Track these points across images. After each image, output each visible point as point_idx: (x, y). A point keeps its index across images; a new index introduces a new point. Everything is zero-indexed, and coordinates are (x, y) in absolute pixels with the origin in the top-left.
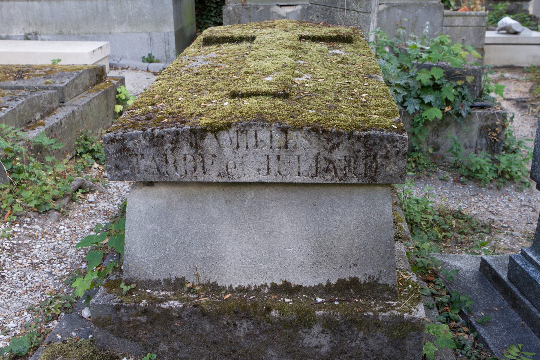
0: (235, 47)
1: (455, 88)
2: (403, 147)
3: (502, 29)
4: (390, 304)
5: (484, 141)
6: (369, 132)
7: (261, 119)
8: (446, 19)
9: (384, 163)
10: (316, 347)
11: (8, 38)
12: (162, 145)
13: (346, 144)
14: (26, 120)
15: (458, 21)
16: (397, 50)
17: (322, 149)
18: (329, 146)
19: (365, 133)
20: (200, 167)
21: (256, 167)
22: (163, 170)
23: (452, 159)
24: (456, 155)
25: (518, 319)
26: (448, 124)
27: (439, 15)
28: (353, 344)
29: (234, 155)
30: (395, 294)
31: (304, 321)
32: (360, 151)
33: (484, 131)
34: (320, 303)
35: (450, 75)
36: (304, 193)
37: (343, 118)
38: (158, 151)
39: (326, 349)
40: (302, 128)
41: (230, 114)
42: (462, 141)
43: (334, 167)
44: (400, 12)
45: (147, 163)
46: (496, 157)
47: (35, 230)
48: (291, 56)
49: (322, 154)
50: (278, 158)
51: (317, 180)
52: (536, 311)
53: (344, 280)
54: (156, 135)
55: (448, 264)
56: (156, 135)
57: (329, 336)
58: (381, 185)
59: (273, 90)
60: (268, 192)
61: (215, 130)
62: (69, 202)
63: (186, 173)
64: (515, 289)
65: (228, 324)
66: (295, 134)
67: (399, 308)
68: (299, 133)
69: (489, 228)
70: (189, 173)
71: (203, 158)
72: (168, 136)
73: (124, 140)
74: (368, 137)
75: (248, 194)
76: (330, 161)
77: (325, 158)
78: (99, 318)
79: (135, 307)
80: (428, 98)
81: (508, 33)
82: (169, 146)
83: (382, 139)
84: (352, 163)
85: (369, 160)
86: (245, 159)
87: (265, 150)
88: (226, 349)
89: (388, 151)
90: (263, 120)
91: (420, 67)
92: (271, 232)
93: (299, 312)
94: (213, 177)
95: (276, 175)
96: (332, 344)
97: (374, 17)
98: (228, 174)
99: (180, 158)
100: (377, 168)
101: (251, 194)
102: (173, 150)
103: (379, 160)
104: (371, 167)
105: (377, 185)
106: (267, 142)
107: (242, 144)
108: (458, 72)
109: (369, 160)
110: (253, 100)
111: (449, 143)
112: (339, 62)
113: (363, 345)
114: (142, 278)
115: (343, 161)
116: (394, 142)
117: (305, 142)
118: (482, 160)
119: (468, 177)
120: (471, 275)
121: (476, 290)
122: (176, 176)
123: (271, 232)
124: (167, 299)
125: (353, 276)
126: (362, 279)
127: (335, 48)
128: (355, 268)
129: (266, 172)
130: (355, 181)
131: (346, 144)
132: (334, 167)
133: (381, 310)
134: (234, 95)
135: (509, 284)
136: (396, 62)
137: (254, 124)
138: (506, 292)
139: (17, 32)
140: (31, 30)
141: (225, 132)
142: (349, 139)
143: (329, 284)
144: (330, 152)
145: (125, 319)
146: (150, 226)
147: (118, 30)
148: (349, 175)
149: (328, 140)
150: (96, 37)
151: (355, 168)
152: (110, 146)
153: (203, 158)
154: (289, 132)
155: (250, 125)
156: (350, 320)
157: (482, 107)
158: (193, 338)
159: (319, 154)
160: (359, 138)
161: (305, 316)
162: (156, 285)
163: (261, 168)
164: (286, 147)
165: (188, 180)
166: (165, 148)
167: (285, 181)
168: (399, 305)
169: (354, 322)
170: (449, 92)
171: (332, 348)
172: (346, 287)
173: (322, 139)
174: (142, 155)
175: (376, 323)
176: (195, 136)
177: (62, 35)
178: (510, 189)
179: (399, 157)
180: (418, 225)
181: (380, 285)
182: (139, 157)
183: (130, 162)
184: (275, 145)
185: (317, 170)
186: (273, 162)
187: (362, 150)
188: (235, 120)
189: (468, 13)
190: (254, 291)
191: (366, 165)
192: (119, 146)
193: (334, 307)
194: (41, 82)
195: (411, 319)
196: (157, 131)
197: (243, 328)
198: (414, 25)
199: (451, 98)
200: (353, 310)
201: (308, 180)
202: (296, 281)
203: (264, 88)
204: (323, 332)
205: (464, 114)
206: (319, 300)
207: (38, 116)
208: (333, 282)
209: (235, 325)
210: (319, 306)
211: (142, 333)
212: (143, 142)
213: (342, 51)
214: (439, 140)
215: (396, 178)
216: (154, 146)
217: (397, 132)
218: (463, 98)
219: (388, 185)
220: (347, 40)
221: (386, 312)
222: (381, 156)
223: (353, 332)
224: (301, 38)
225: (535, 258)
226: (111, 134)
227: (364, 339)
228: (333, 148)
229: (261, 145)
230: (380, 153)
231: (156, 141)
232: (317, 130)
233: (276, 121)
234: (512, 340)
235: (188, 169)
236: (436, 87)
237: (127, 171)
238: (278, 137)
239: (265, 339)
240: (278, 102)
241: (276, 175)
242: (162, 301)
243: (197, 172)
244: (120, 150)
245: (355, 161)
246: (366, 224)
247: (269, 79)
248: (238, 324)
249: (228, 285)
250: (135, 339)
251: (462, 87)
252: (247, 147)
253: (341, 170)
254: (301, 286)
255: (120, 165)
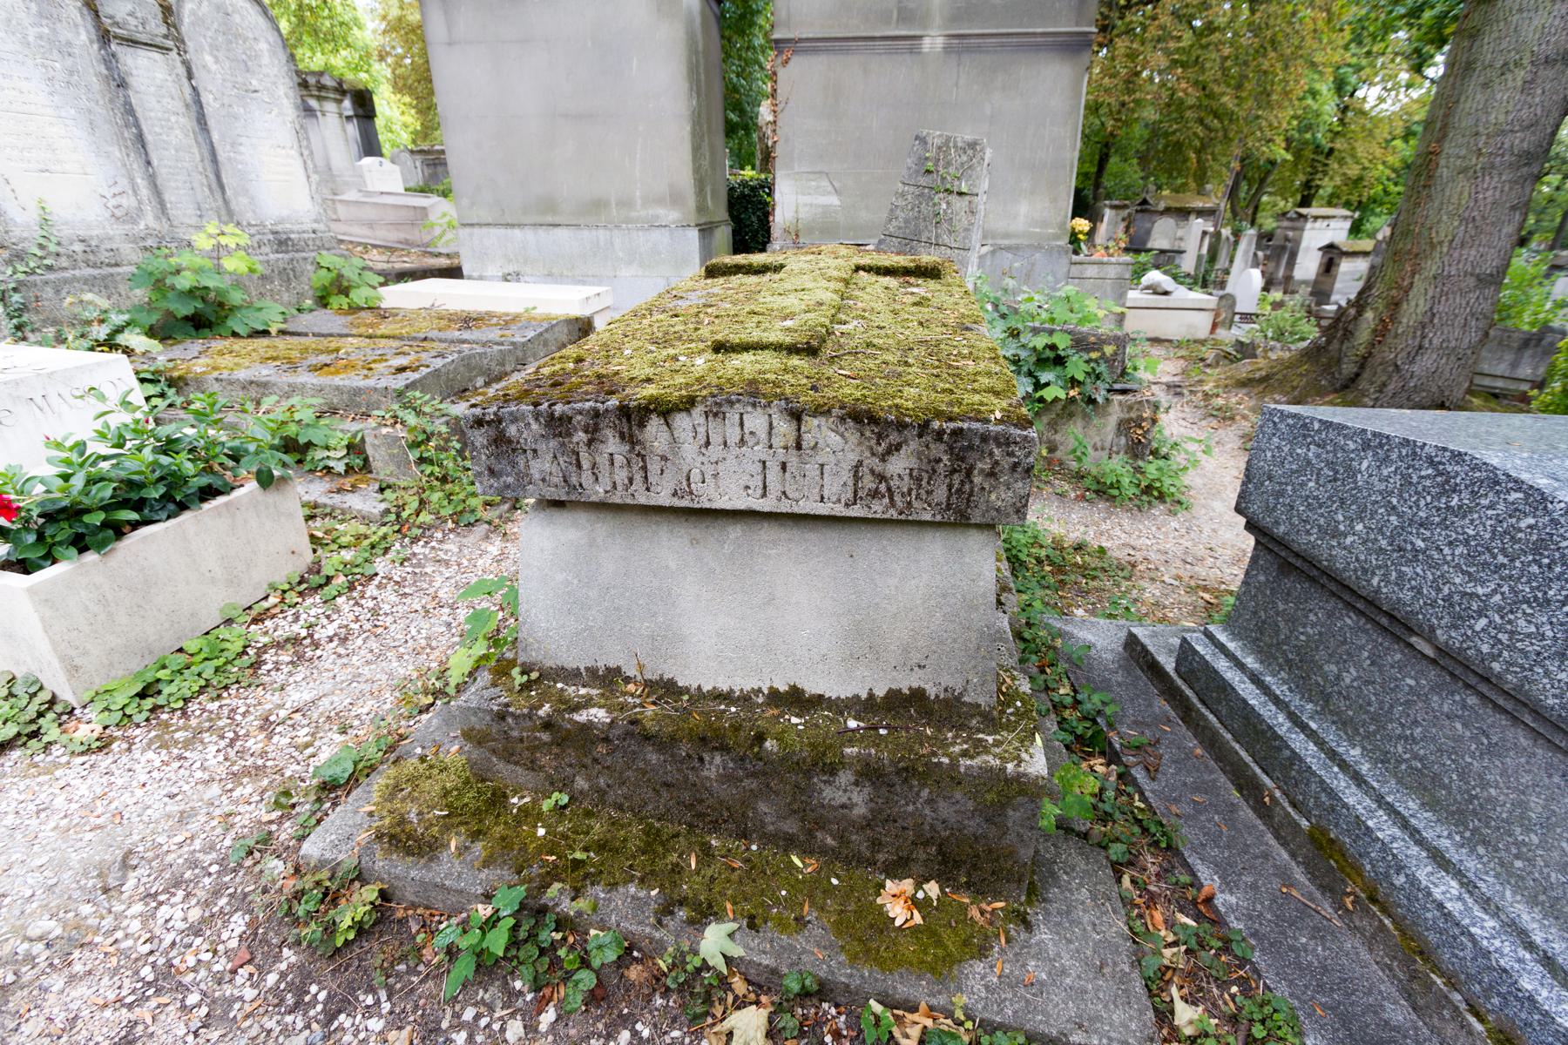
0: (753, 279)
1: (1087, 362)
2: (1027, 456)
3: (1147, 288)
4: (980, 740)
5: (1123, 440)
6: (960, 424)
7: (754, 393)
8: (1074, 268)
9: (987, 486)
10: (843, 806)
11: (481, 278)
12: (570, 435)
13: (914, 444)
14: (457, 387)
15: (1091, 271)
16: (1003, 309)
17: (868, 454)
18: (880, 449)
19: (952, 425)
20: (638, 478)
21: (742, 483)
22: (574, 480)
23: (1074, 465)
24: (1079, 459)
25: (1192, 743)
26: (1071, 415)
27: (1064, 261)
28: (911, 808)
29: (701, 458)
30: (991, 722)
31: (823, 763)
32: (940, 460)
33: (1124, 426)
34: (853, 731)
35: (1081, 343)
36: (833, 536)
37: (914, 395)
38: (563, 444)
39: (860, 810)
40: (829, 411)
41: (699, 380)
42: (1093, 442)
43: (889, 489)
44: (1010, 256)
45: (543, 465)
46: (1140, 463)
47: (446, 552)
48: (836, 292)
49: (866, 462)
50: (784, 467)
51: (857, 511)
52: (1229, 736)
53: (900, 691)
54: (557, 415)
55: (1072, 636)
56: (557, 415)
57: (866, 791)
58: (979, 526)
59: (788, 340)
60: (767, 532)
61: (665, 410)
62: (509, 511)
63: (615, 486)
64: (1189, 692)
65: (689, 756)
66: (816, 422)
67: (997, 750)
68: (822, 420)
69: (1128, 569)
70: (620, 488)
71: (644, 460)
72: (579, 418)
73: (500, 422)
74: (958, 433)
75: (730, 529)
76: (882, 478)
77: (872, 472)
78: (473, 729)
79: (530, 717)
80: (1045, 377)
81: (1155, 293)
82: (581, 436)
83: (985, 438)
84: (924, 483)
85: (957, 479)
86: (721, 467)
87: (760, 451)
88: (686, 796)
89: (997, 463)
90: (755, 394)
91: (1036, 331)
92: (770, 600)
93: (813, 746)
94: (664, 498)
95: (779, 500)
96: (872, 805)
97: (974, 258)
98: (691, 493)
99: (603, 460)
100: (971, 494)
101: (735, 531)
102: (590, 443)
103: (977, 480)
104: (959, 491)
105: (969, 526)
106: (763, 435)
107: (716, 439)
108: (1092, 339)
109: (957, 479)
110: (747, 357)
111: (1072, 443)
112: (915, 304)
113: (927, 811)
114: (549, 663)
115: (906, 478)
116: (1008, 445)
117: (834, 439)
118: (1117, 467)
119: (1097, 492)
120: (1109, 656)
121: (1119, 685)
122: (597, 493)
123: (770, 600)
124: (588, 703)
125: (915, 685)
126: (932, 692)
127: (911, 285)
128: (921, 672)
129: (760, 492)
130: (927, 517)
131: (914, 444)
132: (889, 489)
133: (965, 754)
134: (719, 347)
135: (1179, 682)
136: (1001, 325)
137: (739, 401)
138: (1171, 692)
139: (493, 270)
140: (510, 269)
141: (684, 414)
142: (920, 436)
143: (871, 696)
144: (883, 460)
145: (515, 734)
146: (560, 577)
147: (625, 272)
148: (915, 504)
149: (880, 437)
150: (597, 280)
151: (929, 493)
152: (476, 432)
153: (644, 460)
154: (806, 418)
155: (731, 403)
156: (906, 769)
157: (1124, 392)
158: (629, 773)
159: (860, 463)
160: (939, 434)
161: (824, 754)
162: (573, 676)
163: (750, 484)
164: (799, 447)
165: (618, 501)
166: (575, 439)
167: (796, 510)
168: (997, 744)
169: (914, 772)
170: (1077, 367)
171: (872, 810)
172: (903, 705)
173: (868, 434)
174: (535, 451)
175: (954, 777)
176: (629, 421)
177: (551, 277)
178: (1159, 510)
179: (1016, 475)
180: (1022, 563)
181: (964, 704)
182: (530, 454)
183: (514, 464)
184: (778, 442)
185: (855, 492)
186: (773, 474)
187: (945, 458)
188: (704, 392)
189: (1106, 259)
190: (739, 698)
191: (950, 487)
192: (492, 432)
193: (878, 742)
194: (495, 334)
195: (1019, 776)
196: (559, 408)
197: (715, 765)
198: (1028, 276)
199: (1080, 377)
200: (911, 750)
201: (839, 510)
202: (812, 687)
203: (773, 337)
204: (856, 784)
205: (1100, 400)
206: (852, 724)
207: (480, 382)
208: (880, 692)
209: (701, 760)
210: (849, 736)
211: (544, 760)
212: (535, 426)
213: (923, 288)
214: (1058, 437)
215: (1008, 516)
216: (555, 436)
217: (1016, 426)
218: (1098, 377)
219: (990, 527)
220: (930, 273)
221: (972, 758)
222: (982, 471)
223: (911, 787)
224: (858, 268)
225: (1231, 646)
226: (478, 411)
227: (930, 801)
228: (889, 452)
229: (750, 440)
230: (980, 465)
231: (558, 426)
232: (860, 417)
233: (780, 397)
234: (1185, 784)
235: (619, 482)
236: (1059, 361)
237: (510, 480)
238: (784, 427)
239: (754, 786)
240: (795, 361)
241: (779, 500)
242: (577, 708)
243: (633, 488)
244: (495, 441)
245: (930, 478)
246: (944, 596)
247: (788, 323)
248: (707, 758)
249: (695, 686)
250: (533, 766)
251: (1096, 361)
252: (725, 444)
253: (903, 495)
254: (821, 696)
255: (497, 468)
